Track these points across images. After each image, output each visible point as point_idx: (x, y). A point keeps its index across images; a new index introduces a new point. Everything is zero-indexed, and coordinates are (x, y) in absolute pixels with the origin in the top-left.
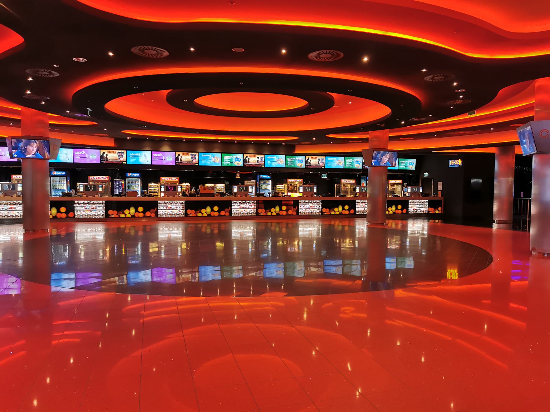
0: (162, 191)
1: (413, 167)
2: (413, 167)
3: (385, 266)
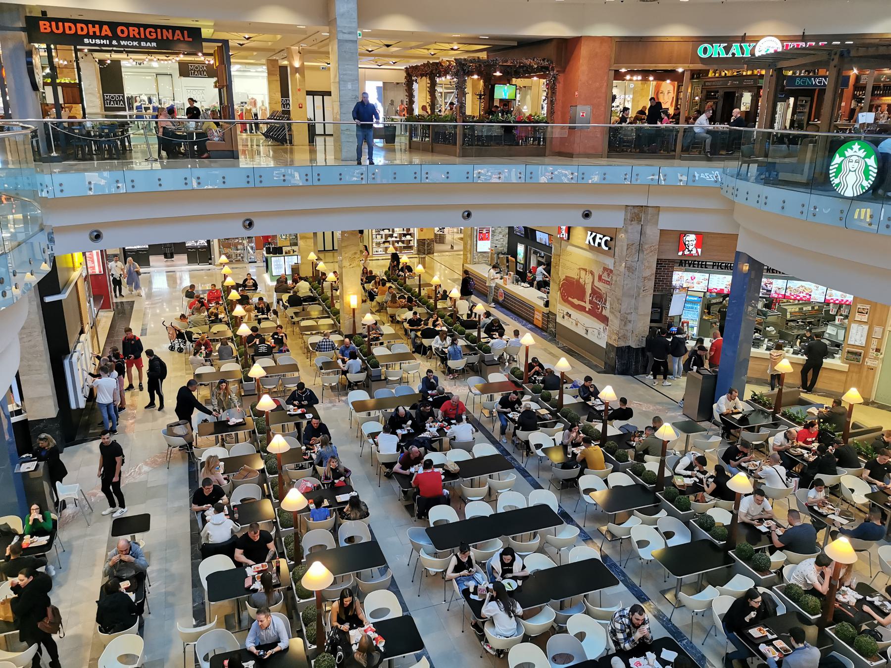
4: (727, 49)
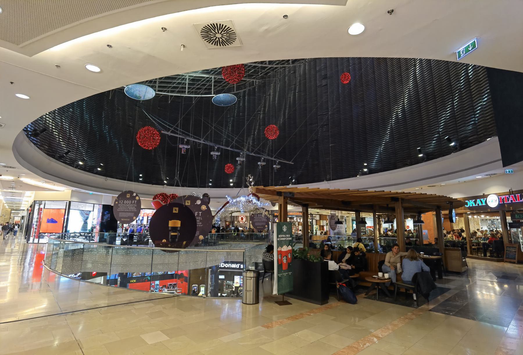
1: (224, 278)
2: (224, 278)
3: (436, 213)
4: (475, 202)
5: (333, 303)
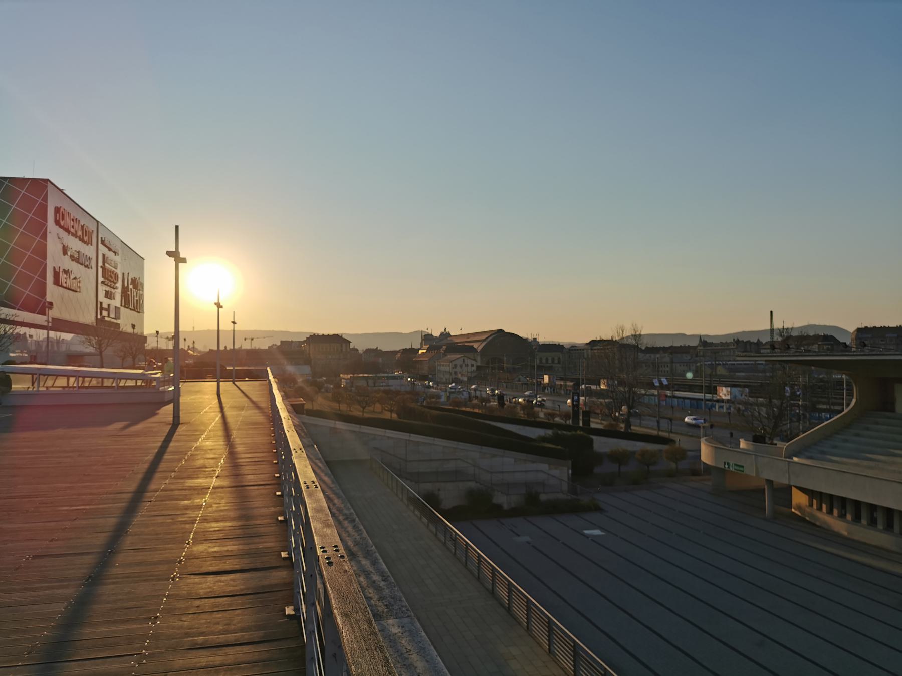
0: (105, 380)
5: (557, 344)
